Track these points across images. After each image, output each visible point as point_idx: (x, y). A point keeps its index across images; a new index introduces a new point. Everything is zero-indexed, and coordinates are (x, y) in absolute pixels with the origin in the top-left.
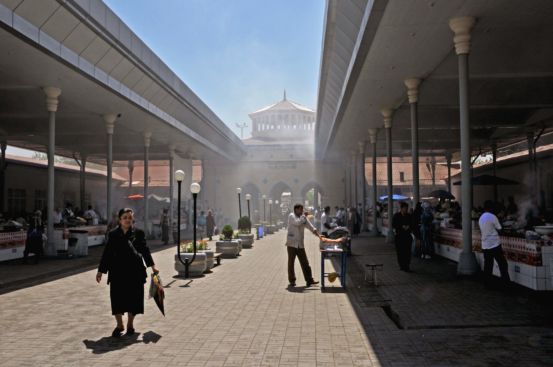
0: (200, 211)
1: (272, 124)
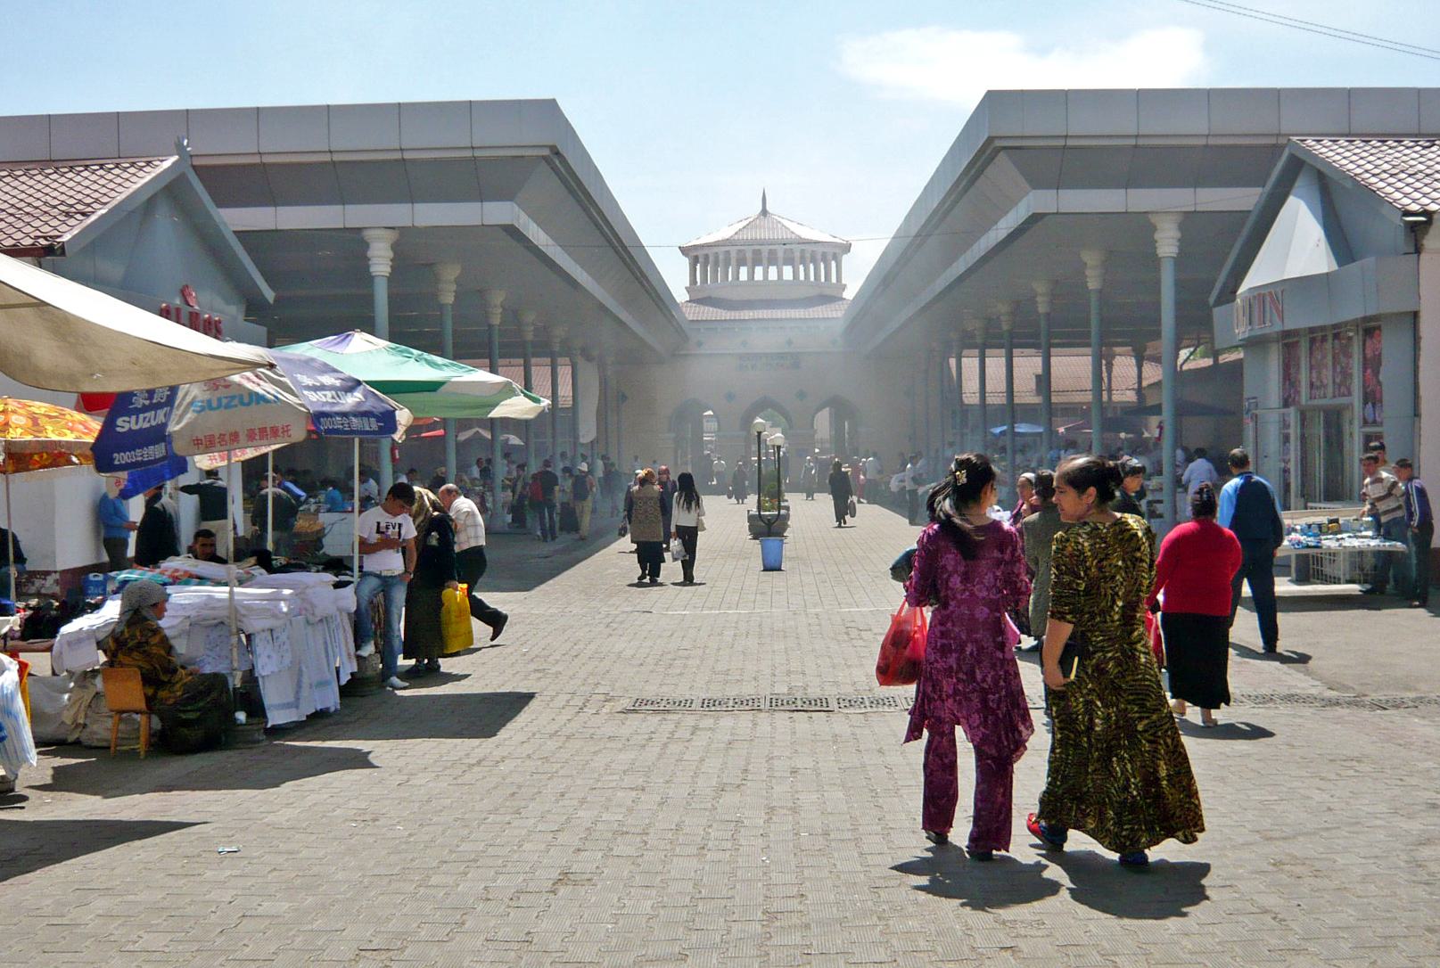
0: (559, 474)
1: (786, 263)
